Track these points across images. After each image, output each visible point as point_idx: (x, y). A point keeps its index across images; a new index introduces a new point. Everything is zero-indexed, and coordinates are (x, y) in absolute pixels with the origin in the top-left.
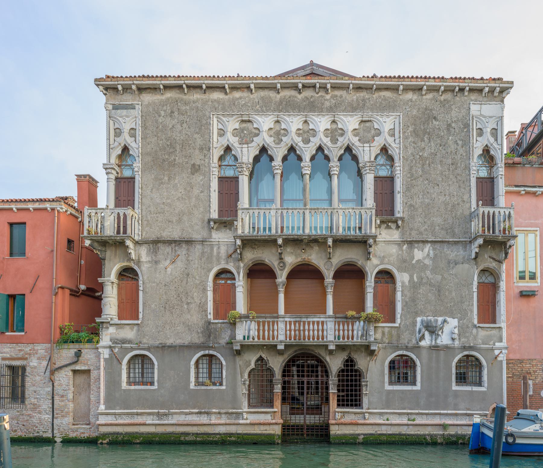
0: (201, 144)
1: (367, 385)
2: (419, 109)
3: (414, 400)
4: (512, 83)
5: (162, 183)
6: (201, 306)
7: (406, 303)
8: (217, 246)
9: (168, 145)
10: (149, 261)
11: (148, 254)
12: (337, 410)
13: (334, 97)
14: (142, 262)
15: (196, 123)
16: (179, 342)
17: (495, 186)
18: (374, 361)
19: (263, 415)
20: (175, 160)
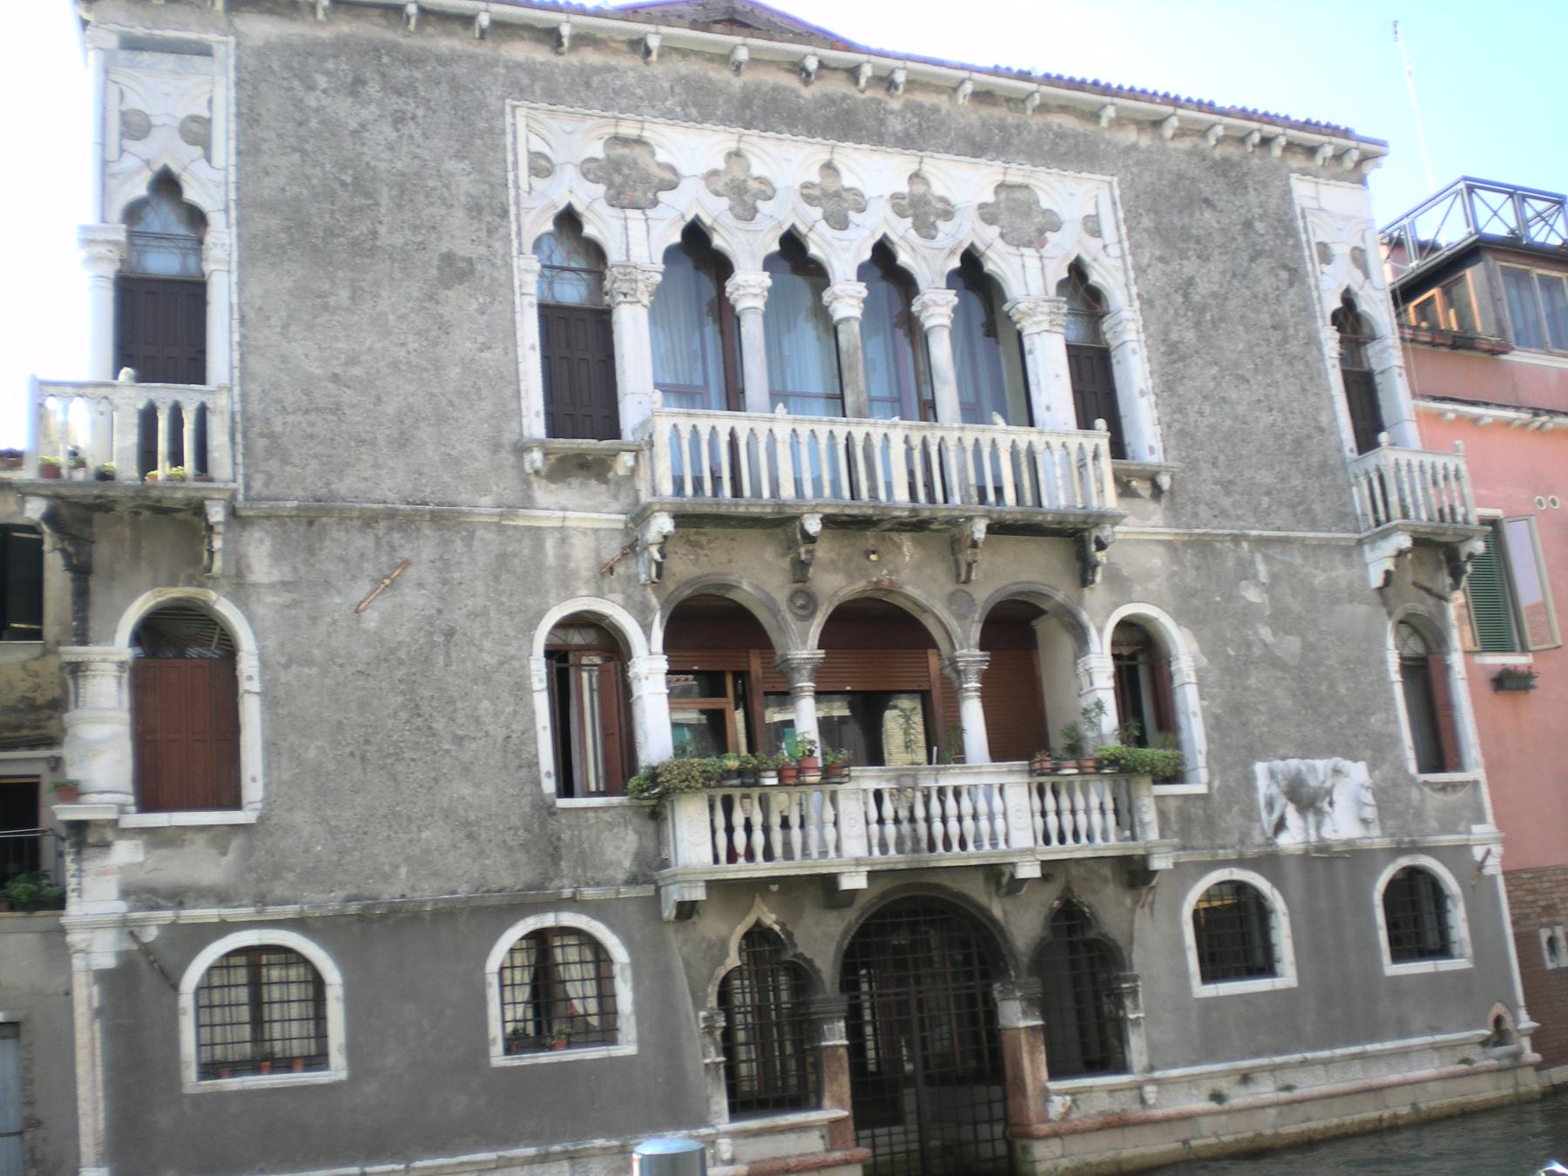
0: (473, 191)
1: (1134, 992)
2: (1160, 173)
3: (1278, 1027)
4: (1383, 144)
5: (326, 307)
6: (511, 747)
7: (1217, 718)
8: (558, 535)
9: (343, 184)
10: (284, 583)
11: (277, 557)
12: (1054, 1086)
13: (916, 108)
14: (255, 585)
15: (451, 125)
16: (428, 892)
17: (1381, 396)
18: (1147, 909)
19: (793, 1136)
20: (374, 234)
